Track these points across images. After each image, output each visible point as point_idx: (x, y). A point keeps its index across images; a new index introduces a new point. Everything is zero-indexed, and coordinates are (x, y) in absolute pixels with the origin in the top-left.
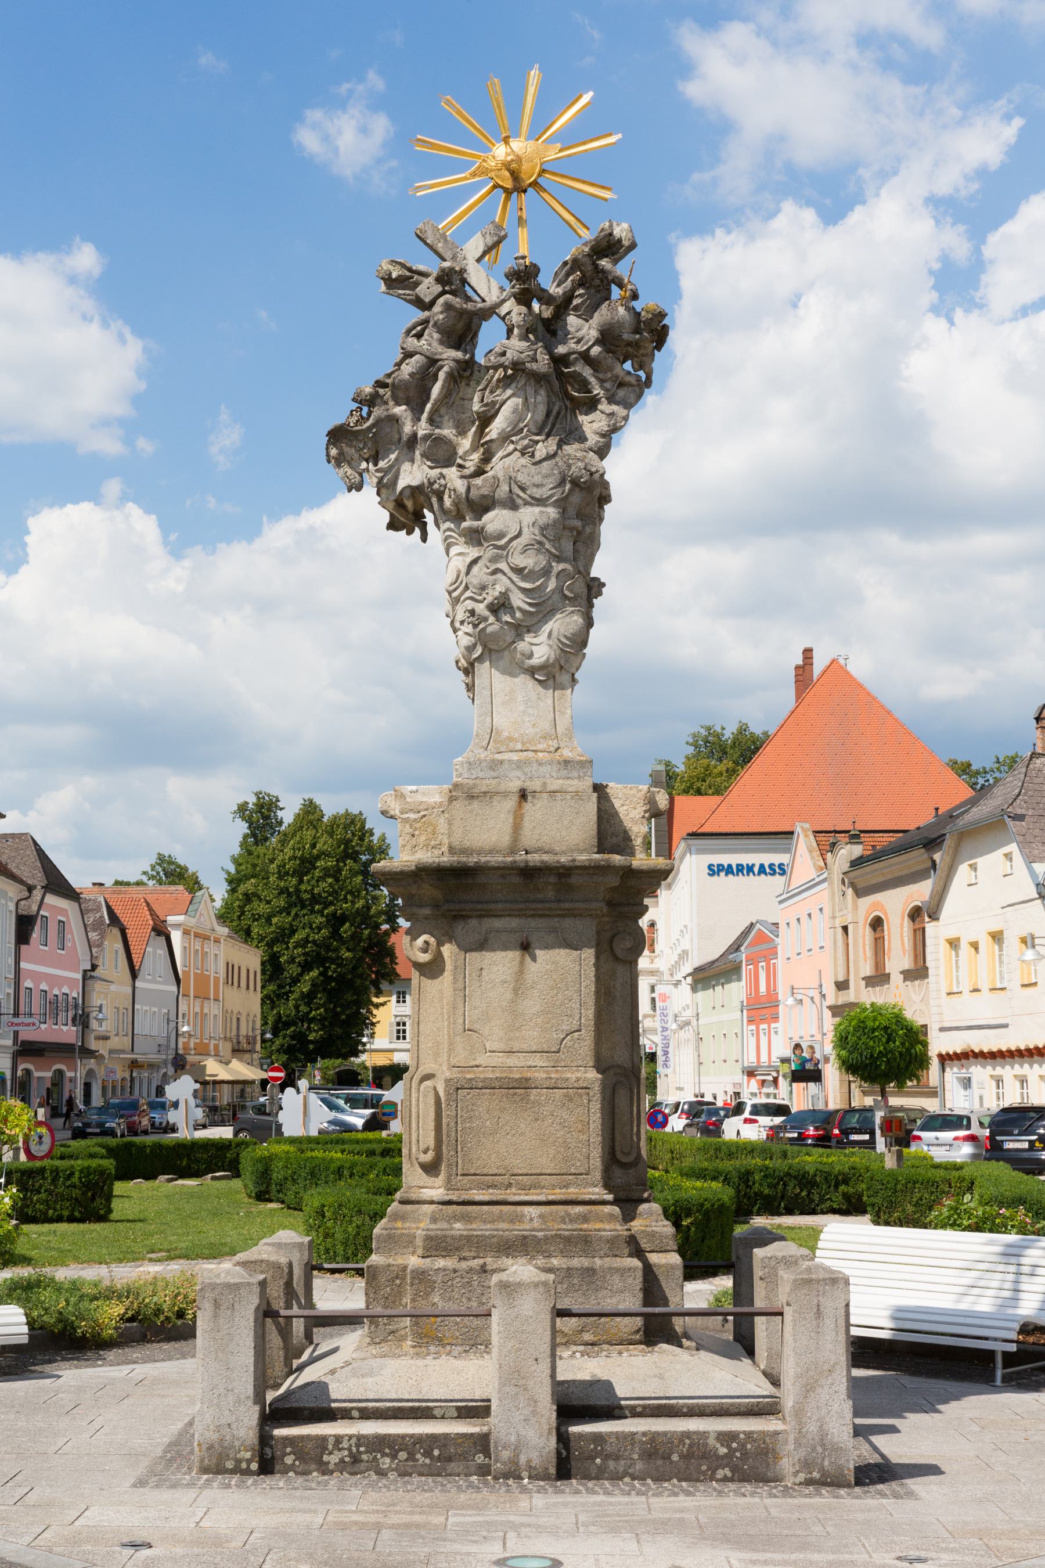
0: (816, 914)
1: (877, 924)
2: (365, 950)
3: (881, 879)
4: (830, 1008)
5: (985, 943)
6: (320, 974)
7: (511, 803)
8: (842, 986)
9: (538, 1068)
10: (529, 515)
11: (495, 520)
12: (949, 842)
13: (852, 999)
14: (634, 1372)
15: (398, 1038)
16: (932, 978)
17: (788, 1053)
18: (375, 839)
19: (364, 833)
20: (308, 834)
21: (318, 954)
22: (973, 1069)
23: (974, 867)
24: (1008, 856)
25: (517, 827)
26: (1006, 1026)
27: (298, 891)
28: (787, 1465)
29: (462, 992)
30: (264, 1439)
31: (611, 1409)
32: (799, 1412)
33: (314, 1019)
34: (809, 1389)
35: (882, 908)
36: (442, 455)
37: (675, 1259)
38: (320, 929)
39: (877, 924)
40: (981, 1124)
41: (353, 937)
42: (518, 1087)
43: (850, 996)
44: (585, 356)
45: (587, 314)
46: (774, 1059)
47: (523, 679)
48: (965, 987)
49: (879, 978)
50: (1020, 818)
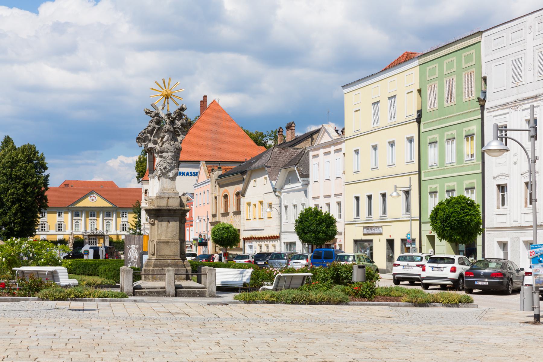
0: (206, 192)
1: (226, 196)
2: (36, 197)
3: (228, 182)
4: (210, 223)
5: (258, 204)
6: (19, 206)
7: (167, 199)
8: (214, 216)
9: (170, 239)
10: (170, 154)
11: (164, 154)
12: (248, 173)
13: (217, 220)
14: (185, 284)
15: (59, 230)
16: (242, 215)
17: (197, 237)
18: (39, 154)
19: (35, 152)
20: (14, 153)
21: (18, 198)
22: (253, 243)
23: (255, 181)
24: (265, 178)
25: (167, 203)
26: (263, 230)
27: (11, 174)
28: (207, 295)
29: (159, 228)
30: (134, 291)
31: (182, 288)
32: (209, 287)
33: (16, 223)
34: (210, 284)
35: (227, 192)
36: (155, 143)
37: (190, 268)
38: (20, 189)
39: (226, 196)
40: (252, 258)
41: (31, 192)
42: (167, 243)
43: (217, 219)
44: (178, 128)
45: (179, 120)
46: (191, 239)
47: (168, 179)
48: (252, 218)
49: (226, 214)
50: (269, 167)
